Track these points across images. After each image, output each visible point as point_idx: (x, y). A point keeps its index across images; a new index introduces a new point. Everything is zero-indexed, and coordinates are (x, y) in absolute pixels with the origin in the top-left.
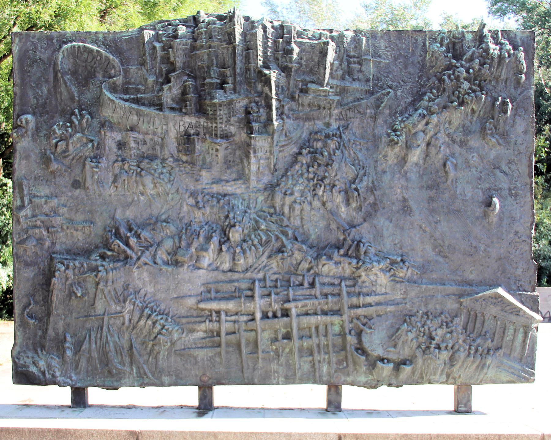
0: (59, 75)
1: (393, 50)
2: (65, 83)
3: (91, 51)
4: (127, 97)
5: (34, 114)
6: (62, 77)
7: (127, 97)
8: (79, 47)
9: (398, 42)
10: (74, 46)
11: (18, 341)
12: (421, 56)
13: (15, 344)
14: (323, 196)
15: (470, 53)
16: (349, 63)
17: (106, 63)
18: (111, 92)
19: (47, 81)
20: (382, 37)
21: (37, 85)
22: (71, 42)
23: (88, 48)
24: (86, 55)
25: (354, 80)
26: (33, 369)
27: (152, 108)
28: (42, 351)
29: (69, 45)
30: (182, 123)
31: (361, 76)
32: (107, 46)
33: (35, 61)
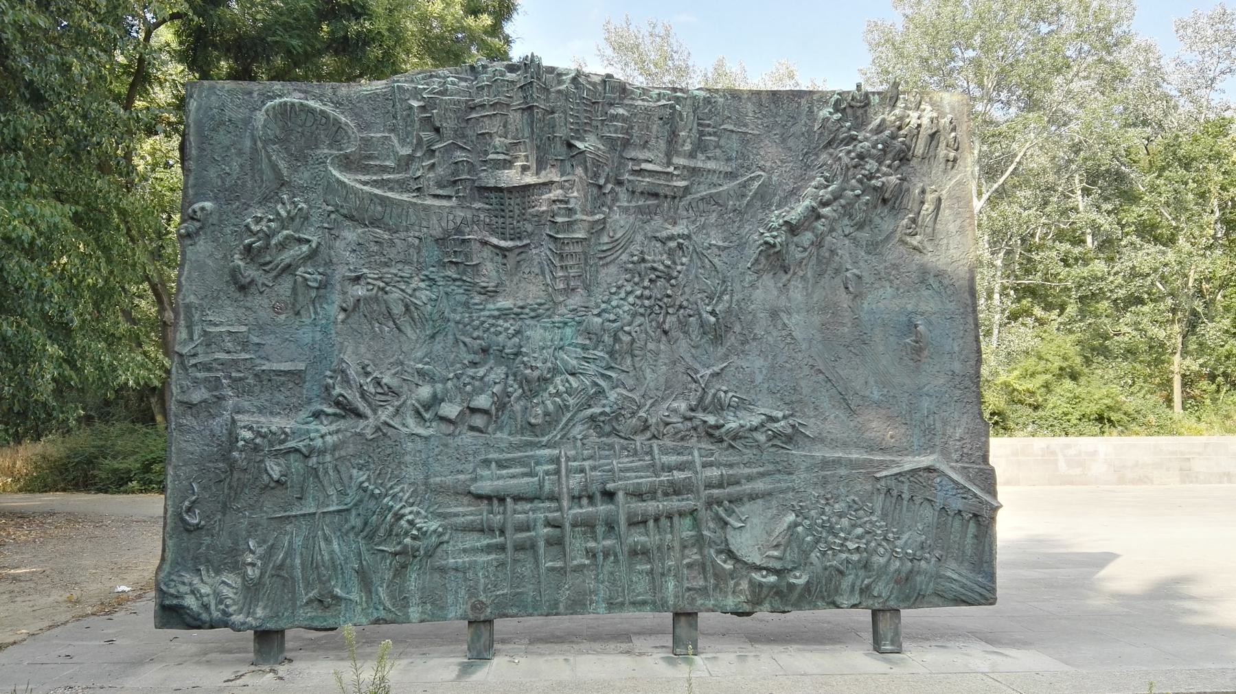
0: (260, 144)
1: (764, 116)
2: (269, 157)
3: (312, 111)
4: (367, 178)
5: (216, 199)
6: (264, 148)
7: (367, 178)
8: (293, 104)
9: (772, 106)
10: (285, 103)
11: (169, 555)
12: (806, 125)
13: (163, 559)
14: (664, 322)
15: (878, 121)
16: (702, 134)
17: (334, 129)
18: (341, 171)
19: (240, 153)
20: (749, 99)
21: (223, 158)
22: (280, 96)
23: (307, 106)
24: (303, 117)
25: (709, 158)
26: (190, 602)
27: (1127, 576)
28: (208, 571)
29: (278, 101)
30: (451, 217)
31: (718, 152)
32: (98, 521)
33: (222, 123)
